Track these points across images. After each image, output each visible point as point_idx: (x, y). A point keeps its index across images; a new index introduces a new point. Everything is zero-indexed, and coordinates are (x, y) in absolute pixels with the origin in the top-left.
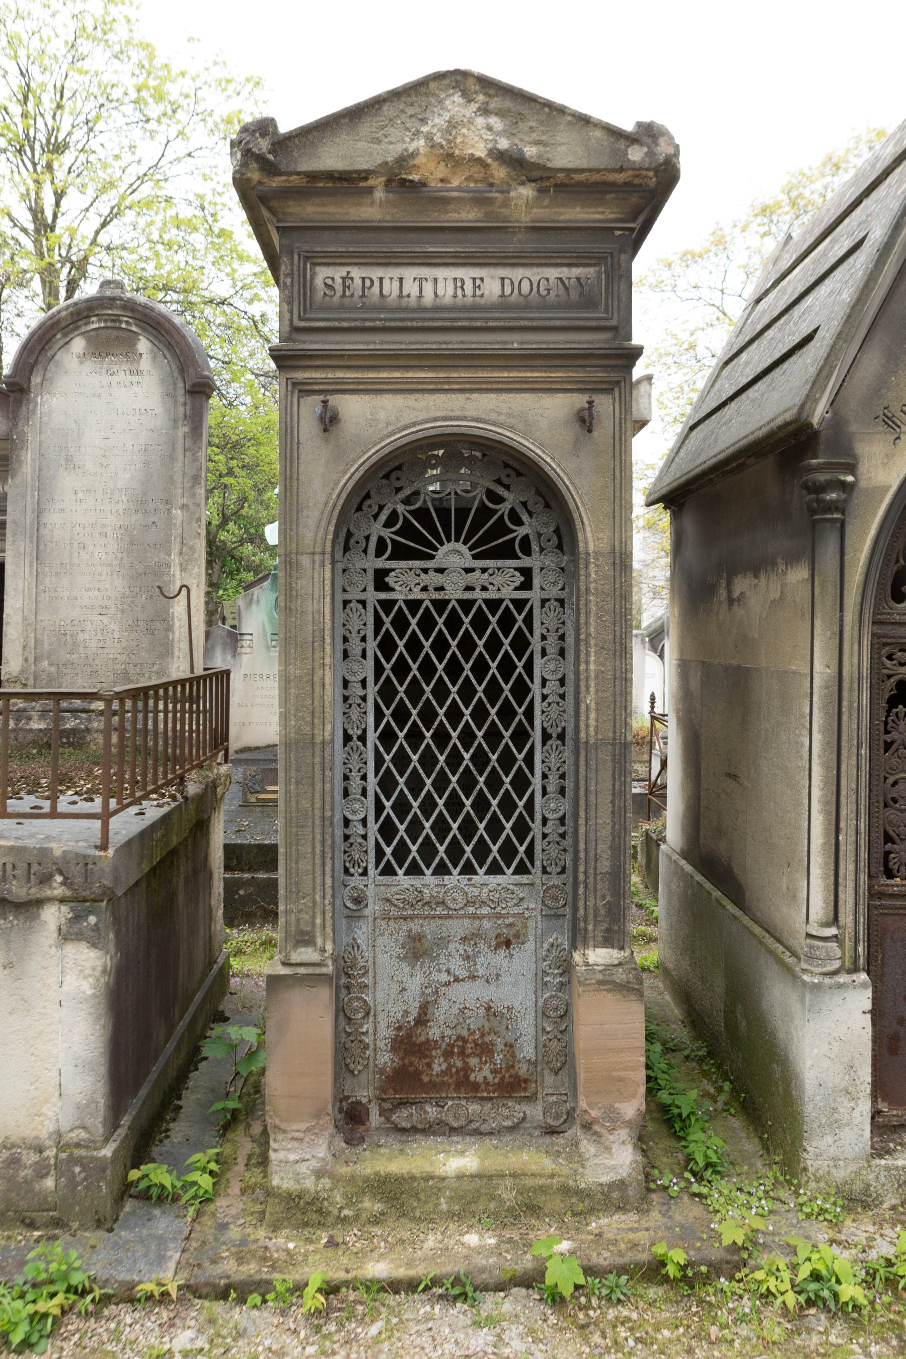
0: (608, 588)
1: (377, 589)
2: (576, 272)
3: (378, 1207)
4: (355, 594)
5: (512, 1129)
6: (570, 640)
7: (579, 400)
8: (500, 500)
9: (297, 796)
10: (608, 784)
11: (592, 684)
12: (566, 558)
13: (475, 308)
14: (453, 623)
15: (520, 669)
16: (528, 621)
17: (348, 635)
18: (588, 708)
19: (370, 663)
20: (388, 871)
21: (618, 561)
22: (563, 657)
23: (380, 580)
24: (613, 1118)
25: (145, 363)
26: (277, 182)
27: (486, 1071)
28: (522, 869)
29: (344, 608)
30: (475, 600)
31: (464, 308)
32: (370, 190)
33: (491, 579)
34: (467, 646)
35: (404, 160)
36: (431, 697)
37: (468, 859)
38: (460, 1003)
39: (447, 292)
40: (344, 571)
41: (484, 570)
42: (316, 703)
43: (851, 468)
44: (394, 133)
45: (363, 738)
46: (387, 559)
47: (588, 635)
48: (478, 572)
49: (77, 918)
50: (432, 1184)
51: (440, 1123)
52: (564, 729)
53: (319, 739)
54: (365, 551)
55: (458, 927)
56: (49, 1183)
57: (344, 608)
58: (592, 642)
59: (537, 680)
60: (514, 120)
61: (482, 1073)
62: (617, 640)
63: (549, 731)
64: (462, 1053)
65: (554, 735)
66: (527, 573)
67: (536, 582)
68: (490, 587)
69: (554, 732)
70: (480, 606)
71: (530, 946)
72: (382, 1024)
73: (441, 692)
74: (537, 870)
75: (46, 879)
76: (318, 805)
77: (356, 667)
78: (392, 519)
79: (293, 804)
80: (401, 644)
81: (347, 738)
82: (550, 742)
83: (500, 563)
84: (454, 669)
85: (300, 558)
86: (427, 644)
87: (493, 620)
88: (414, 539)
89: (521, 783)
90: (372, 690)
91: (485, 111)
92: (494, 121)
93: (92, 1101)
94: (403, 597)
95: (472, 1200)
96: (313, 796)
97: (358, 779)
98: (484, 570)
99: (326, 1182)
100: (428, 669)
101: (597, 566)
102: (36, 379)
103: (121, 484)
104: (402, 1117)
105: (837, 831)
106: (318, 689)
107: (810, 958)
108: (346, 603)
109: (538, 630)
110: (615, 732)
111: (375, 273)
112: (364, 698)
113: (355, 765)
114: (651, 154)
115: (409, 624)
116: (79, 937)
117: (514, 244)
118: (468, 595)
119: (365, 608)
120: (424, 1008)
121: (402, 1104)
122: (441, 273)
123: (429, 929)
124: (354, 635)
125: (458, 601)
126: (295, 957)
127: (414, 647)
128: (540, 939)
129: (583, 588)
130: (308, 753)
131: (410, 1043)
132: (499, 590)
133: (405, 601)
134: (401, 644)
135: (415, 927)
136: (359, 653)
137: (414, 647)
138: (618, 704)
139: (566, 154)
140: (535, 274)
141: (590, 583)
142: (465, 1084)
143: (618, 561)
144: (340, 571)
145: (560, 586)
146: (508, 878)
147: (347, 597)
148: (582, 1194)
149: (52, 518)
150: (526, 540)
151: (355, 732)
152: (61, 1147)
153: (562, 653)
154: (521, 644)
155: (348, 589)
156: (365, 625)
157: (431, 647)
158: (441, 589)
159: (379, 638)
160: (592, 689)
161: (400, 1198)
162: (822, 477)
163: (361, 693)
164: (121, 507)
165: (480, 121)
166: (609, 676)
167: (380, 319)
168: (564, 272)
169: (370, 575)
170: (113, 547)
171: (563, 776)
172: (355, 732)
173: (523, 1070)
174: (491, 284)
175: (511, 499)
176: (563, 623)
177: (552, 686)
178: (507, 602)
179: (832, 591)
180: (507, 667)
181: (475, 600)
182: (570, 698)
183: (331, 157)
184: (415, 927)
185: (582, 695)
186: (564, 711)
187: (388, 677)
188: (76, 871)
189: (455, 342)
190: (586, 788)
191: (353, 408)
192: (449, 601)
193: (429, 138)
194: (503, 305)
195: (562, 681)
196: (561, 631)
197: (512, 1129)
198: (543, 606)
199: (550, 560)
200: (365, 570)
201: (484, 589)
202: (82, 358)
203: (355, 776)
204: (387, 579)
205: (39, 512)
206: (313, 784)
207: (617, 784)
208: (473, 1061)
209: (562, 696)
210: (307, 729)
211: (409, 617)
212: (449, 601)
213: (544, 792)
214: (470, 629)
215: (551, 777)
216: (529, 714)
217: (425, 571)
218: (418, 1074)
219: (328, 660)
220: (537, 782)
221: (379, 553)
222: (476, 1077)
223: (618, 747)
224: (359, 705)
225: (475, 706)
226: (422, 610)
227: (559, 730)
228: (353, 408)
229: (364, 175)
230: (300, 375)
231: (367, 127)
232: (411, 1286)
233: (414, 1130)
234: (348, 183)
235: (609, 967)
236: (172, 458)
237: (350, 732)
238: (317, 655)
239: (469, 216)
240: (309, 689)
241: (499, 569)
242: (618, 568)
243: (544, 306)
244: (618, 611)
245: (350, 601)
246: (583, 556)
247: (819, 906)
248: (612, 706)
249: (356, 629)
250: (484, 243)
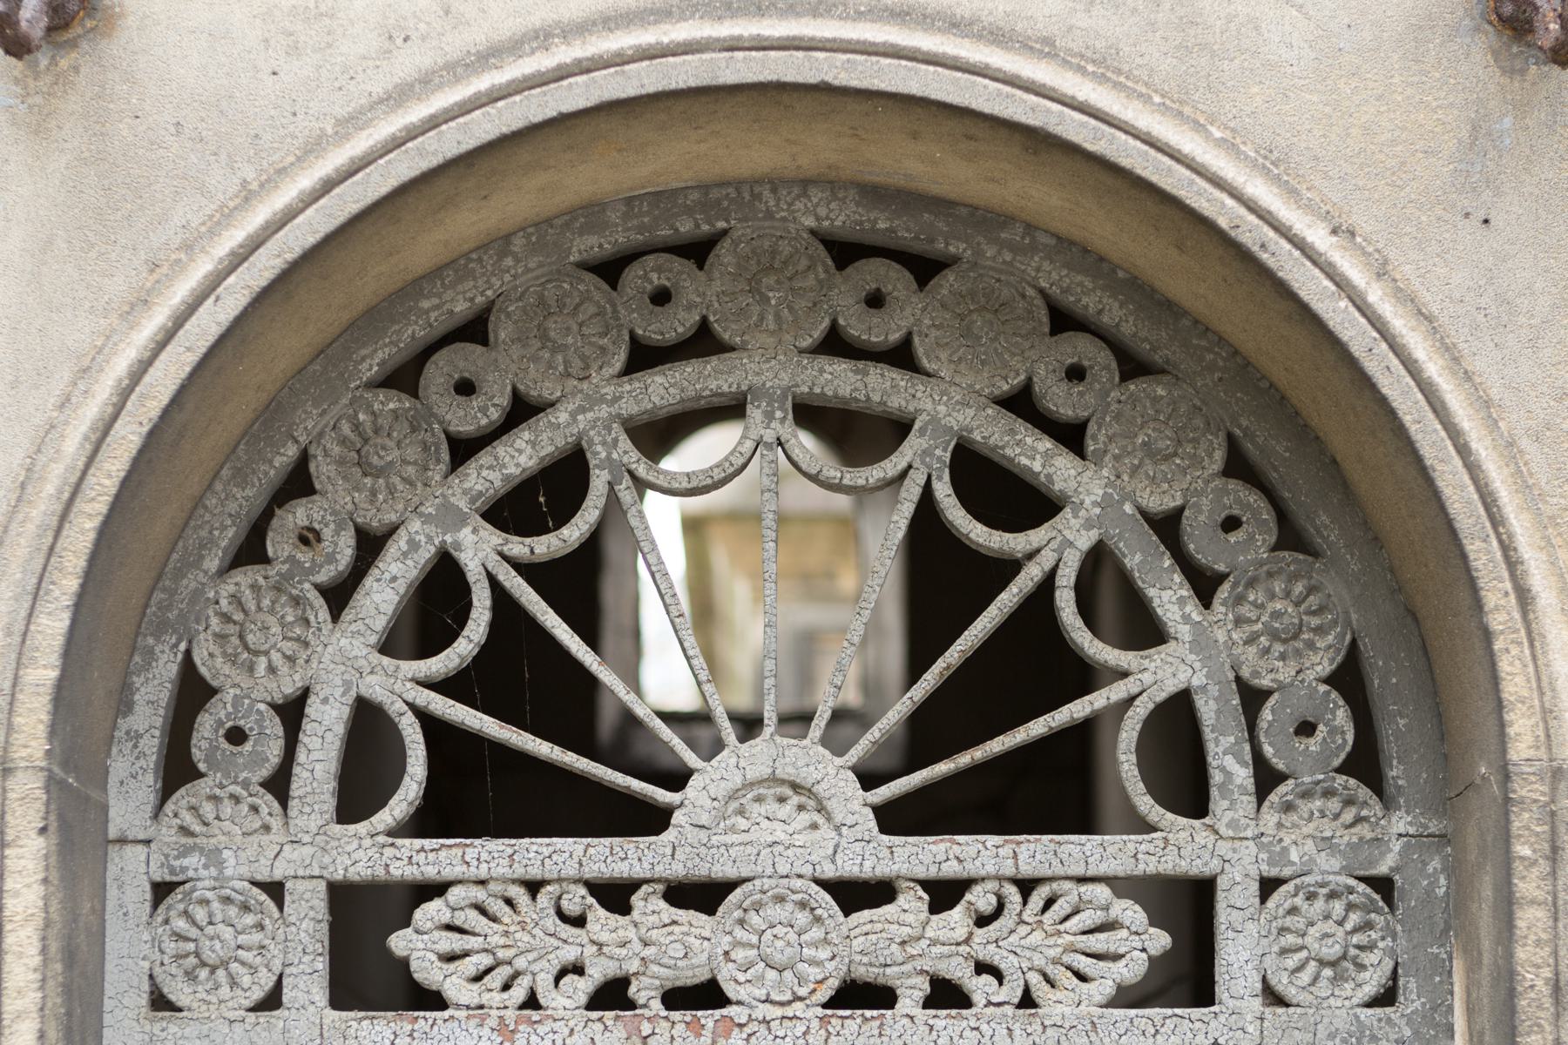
8: (1027, 504)
66: (1189, 907)
78: (438, 600)
150: (1176, 722)
175: (1091, 502)
199: (1313, 836)
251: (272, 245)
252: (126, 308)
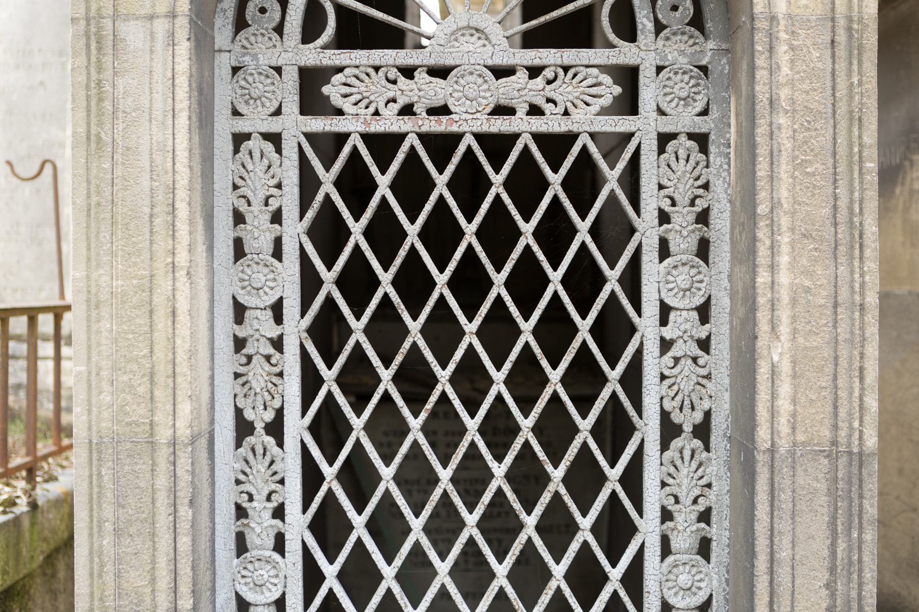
0: (819, 101)
1: (305, 110)
4: (257, 121)
6: (721, 222)
9: (118, 560)
10: (821, 545)
11: (784, 315)
12: (711, 45)
14: (470, 185)
15: (329, 375)
17: (243, 208)
18: (774, 372)
19: (291, 267)
21: (842, 37)
22: (706, 260)
23: (312, 89)
29: (236, 151)
30: (516, 136)
33: (549, 91)
34: (498, 235)
36: (422, 343)
37: (471, 541)
40: (235, 70)
41: (534, 72)
42: (160, 354)
45: (276, 429)
46: (325, 47)
47: (775, 205)
48: (522, 76)
52: (708, 414)
53: (164, 435)
54: (279, 30)
57: (236, 151)
58: (785, 222)
59: (650, 308)
62: (842, 216)
63: (676, 418)
65: (688, 428)
66: (628, 77)
67: (648, 94)
68: (548, 108)
69: (688, 420)
70: (526, 148)
73: (443, 332)
76: (164, 583)
77: (259, 277)
79: (109, 578)
80: (386, 278)
81: (244, 428)
82: (676, 443)
83: (569, 55)
84: (470, 283)
85: (122, 27)
86: (413, 230)
87: (555, 179)
89: (616, 530)
90: (296, 327)
94: (362, 128)
96: (153, 562)
97: (267, 514)
98: (534, 72)
100: (414, 284)
101: (792, 48)
106: (162, 321)
108: (239, 139)
110: (835, 427)
112: (278, 344)
113: (260, 485)
115: (374, 187)
118: (500, 125)
119: (279, 151)
124: (257, 207)
125: (478, 137)
127: (385, 235)
129: (762, 98)
130: (143, 466)
132: (566, 113)
133: (366, 137)
134: (386, 278)
136: (269, 248)
137: (385, 235)
138: (843, 363)
141: (780, 86)
143: (842, 37)
144: (227, 72)
145: (699, 106)
147: (242, 126)
151: (260, 417)
153: (703, 250)
154: (614, 232)
155: (242, 108)
156: (279, 186)
157: (422, 235)
158: (443, 110)
159: (310, 214)
160: (784, 330)
163: (273, 331)
166: (822, 298)
169: (291, 78)
171: (705, 517)
172: (260, 417)
176: (706, 186)
177: (683, 323)
178: (584, 139)
180: (584, 280)
181: (516, 136)
182: (721, 346)
185: (760, 343)
186: (708, 377)
187: (329, 300)
190: (772, 554)
192: (458, 137)
195: (704, 312)
196: (701, 204)
198: (661, 150)
199: (678, 50)
200: (278, 70)
201: (535, 111)
203: (261, 512)
204: (326, 90)
206: (153, 535)
207: (842, 545)
209: (704, 345)
210: (139, 412)
211: (374, 170)
212: (458, 137)
213: (666, 549)
214: (505, 197)
215: (679, 518)
216: (633, 380)
217: (408, 72)
219: (182, 258)
220: (648, 528)
221: (309, 33)
223: (843, 461)
224: (268, 358)
225: (516, 364)
226: (400, 156)
227: (698, 417)
237: (249, 415)
238: (162, 244)
240: (143, 320)
241: (566, 69)
242: (841, 52)
244: (842, 150)
245: (247, 136)
246: (762, 24)
248: (829, 369)
249: (261, 195)
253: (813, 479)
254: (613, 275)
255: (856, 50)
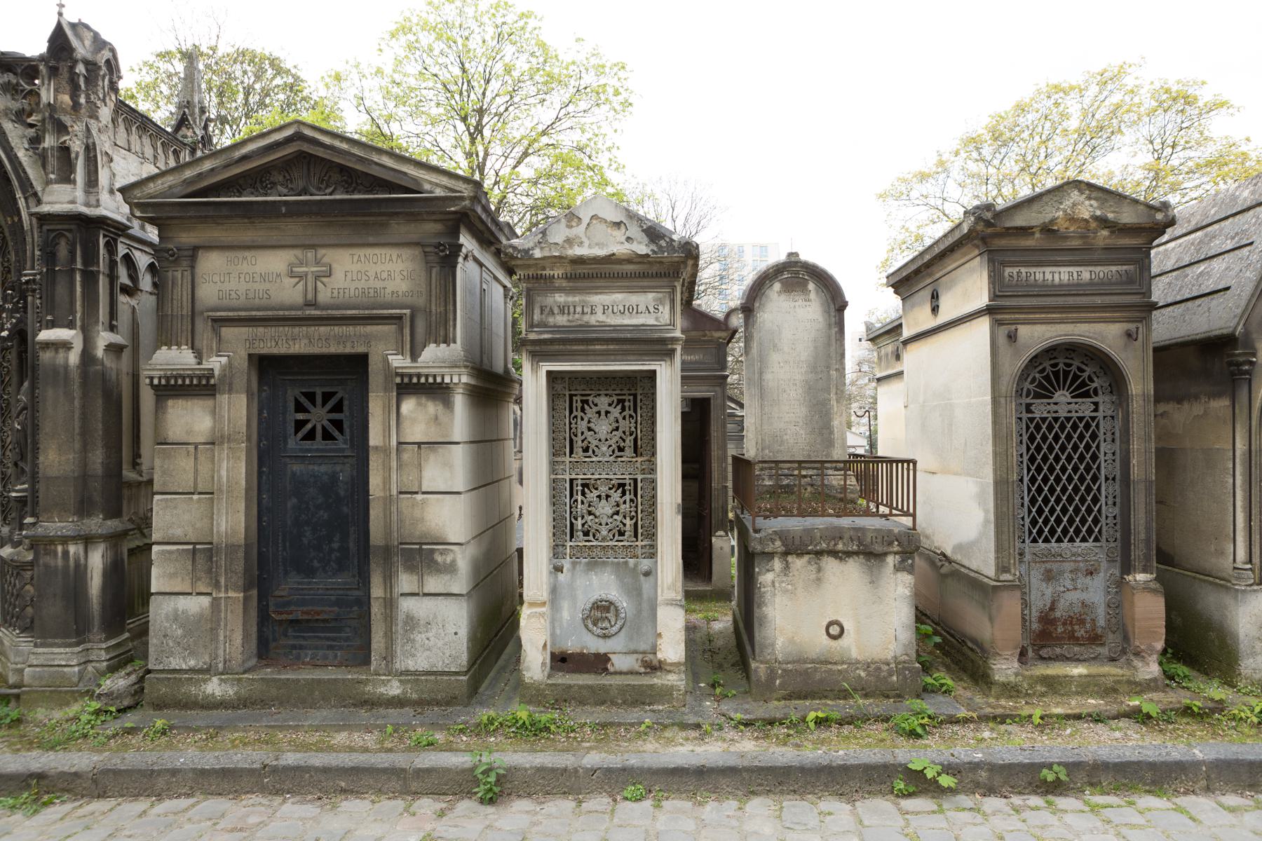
2: (1125, 267)
3: (1044, 689)
5: (1093, 659)
7: (1126, 326)
8: (1083, 371)
13: (1078, 285)
16: (1097, 426)
19: (1024, 446)
20: (1035, 541)
24: (1151, 650)
25: (813, 295)
26: (989, 230)
27: (1082, 632)
28: (1096, 540)
31: (1073, 285)
32: (1033, 234)
35: (1053, 221)
38: (1070, 600)
39: (1065, 277)
43: (1254, 355)
44: (1048, 209)
49: (903, 561)
50: (1069, 679)
51: (1062, 655)
55: (1068, 566)
56: (895, 678)
60: (1102, 202)
61: (1080, 632)
64: (1071, 623)
66: (1096, 404)
71: (1102, 574)
72: (1034, 610)
74: (1103, 540)
75: (890, 544)
78: (1034, 380)
88: (1044, 392)
91: (1089, 198)
92: (1093, 202)
93: (910, 642)
95: (1087, 687)
99: (1020, 678)
102: (757, 305)
103: (803, 358)
104: (1044, 652)
105: (1250, 520)
107: (1238, 578)
109: (1102, 430)
111: (1032, 270)
114: (1166, 216)
116: (904, 569)
117: (1096, 256)
120: (1053, 603)
121: (1043, 647)
122: (1062, 269)
123: (1055, 566)
126: (1002, 578)
128: (1106, 571)
131: (1047, 619)
135: (1048, 566)
139: (1127, 216)
140: (1106, 269)
142: (1073, 638)
146: (1090, 544)
148: (1136, 683)
149: (768, 376)
150: (1096, 389)
152: (897, 663)
153: (1113, 440)
161: (1053, 685)
162: (1241, 359)
164: (803, 370)
165: (1087, 202)
167: (1036, 291)
168: (1119, 268)
170: (800, 391)
173: (1099, 631)
174: (1086, 274)
175: (1088, 371)
177: (1109, 456)
179: (1246, 411)
183: (1019, 220)
184: (1048, 566)
188: (904, 540)
189: (1071, 301)
191: (1024, 331)
193: (1065, 211)
194: (1091, 283)
197: (1093, 659)
199: (1107, 398)
202: (780, 293)
205: (761, 373)
208: (1076, 627)
216: (1098, 468)
218: (1050, 633)
220: (1103, 499)
222: (1078, 634)
228: (1024, 331)
229: (1032, 228)
230: (999, 317)
231: (1035, 207)
232: (1078, 717)
233: (1050, 659)
234: (1024, 231)
235: (1146, 582)
236: (829, 345)
239: (1075, 243)
243: (1111, 284)
247: (1241, 554)
250: (1083, 255)
251: (360, 242)
252: (267, 101)
253: (1142, 486)
254: (1032, 429)
255: (1149, 401)
